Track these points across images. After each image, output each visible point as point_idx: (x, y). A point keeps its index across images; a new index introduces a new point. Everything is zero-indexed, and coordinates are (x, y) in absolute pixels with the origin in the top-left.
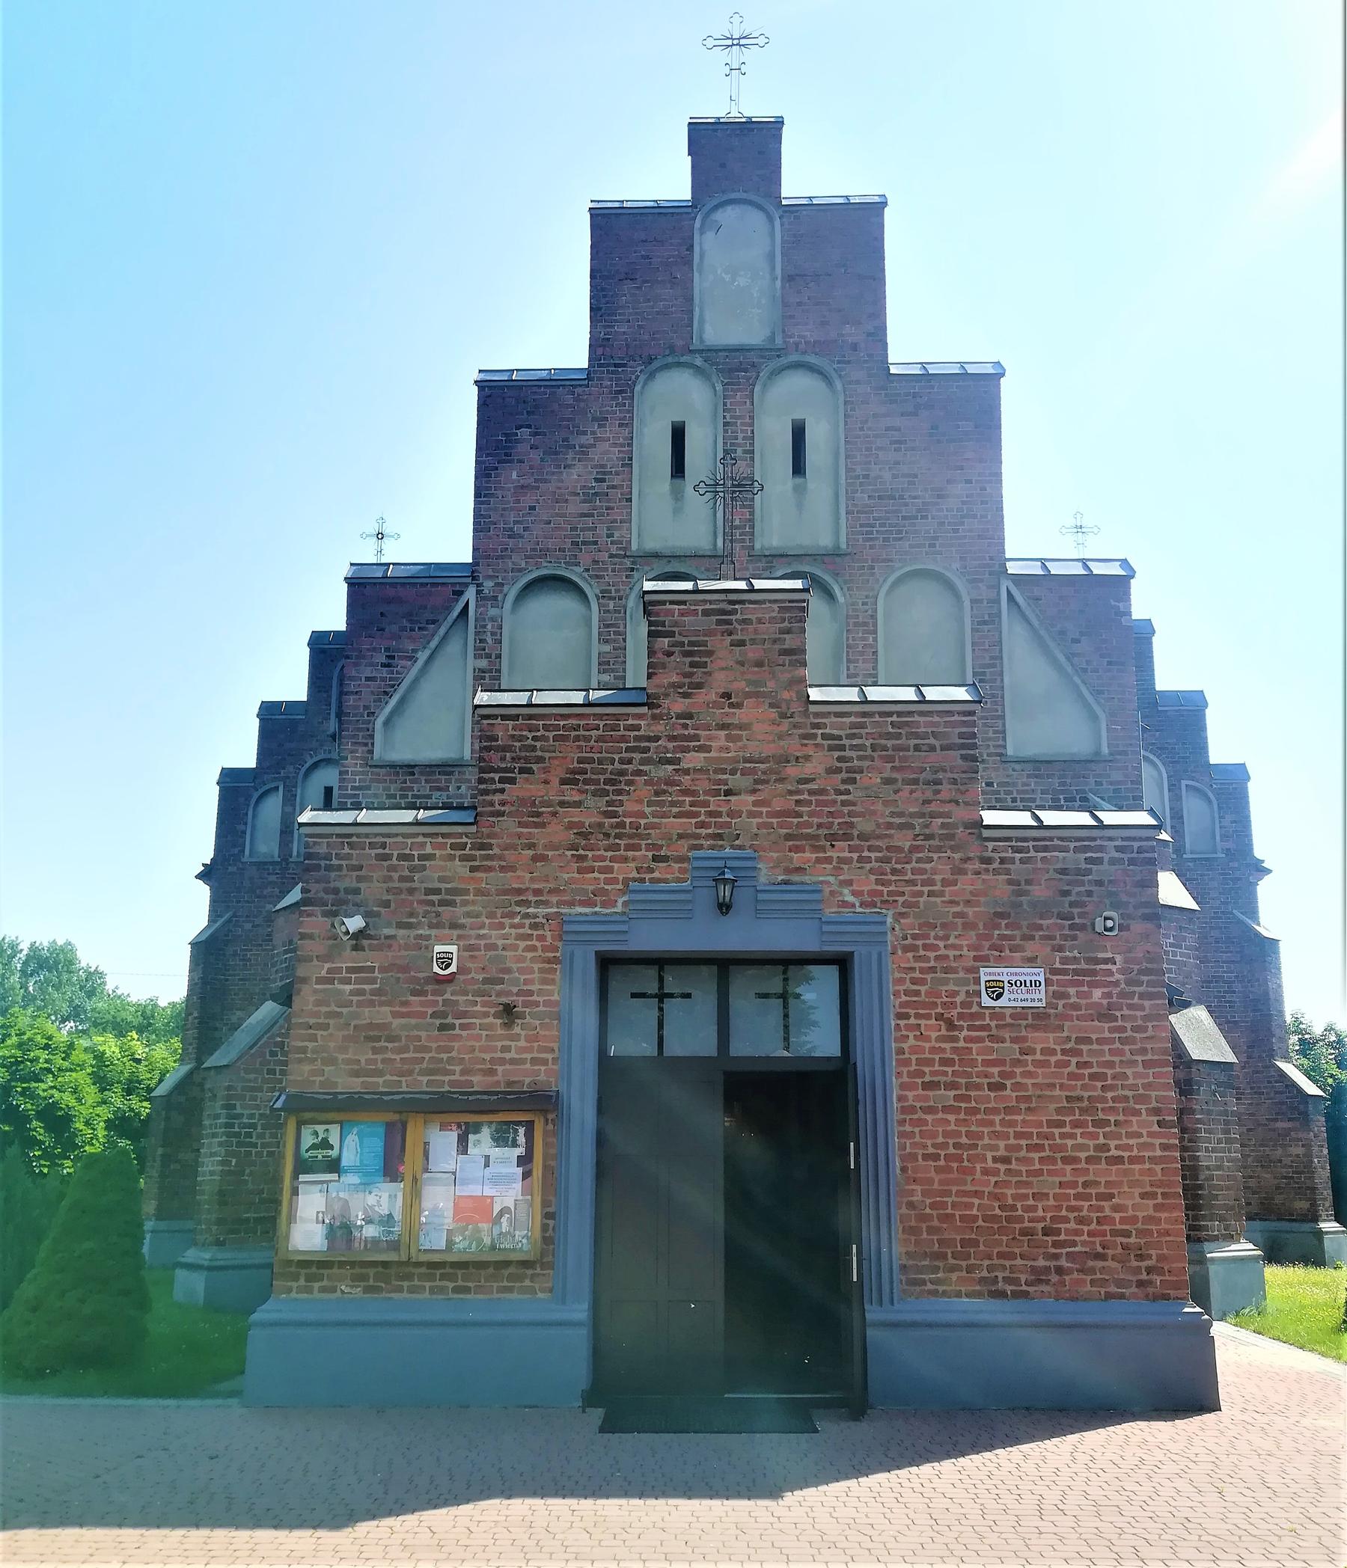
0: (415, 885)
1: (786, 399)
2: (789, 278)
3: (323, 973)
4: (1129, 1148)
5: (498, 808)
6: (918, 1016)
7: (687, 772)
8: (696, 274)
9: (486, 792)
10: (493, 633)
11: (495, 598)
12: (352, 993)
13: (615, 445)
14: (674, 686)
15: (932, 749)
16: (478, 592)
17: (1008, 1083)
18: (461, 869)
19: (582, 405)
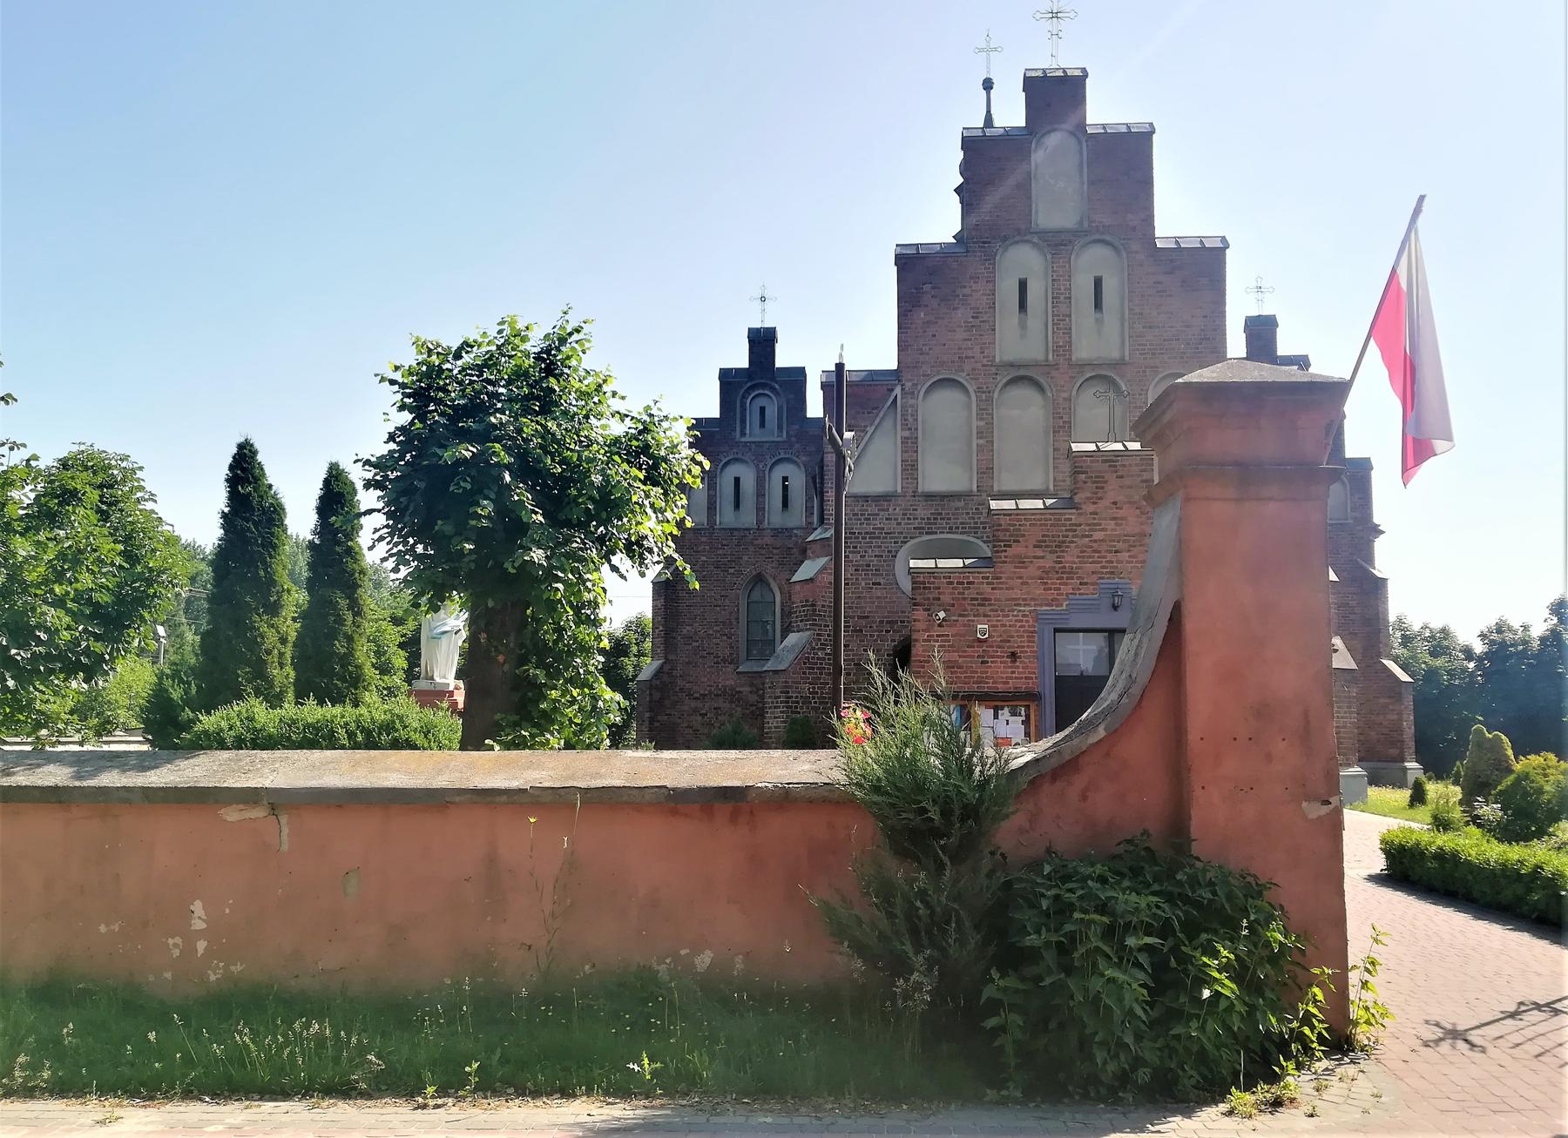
1: (1091, 262)
2: (1091, 183)
18: (988, 589)
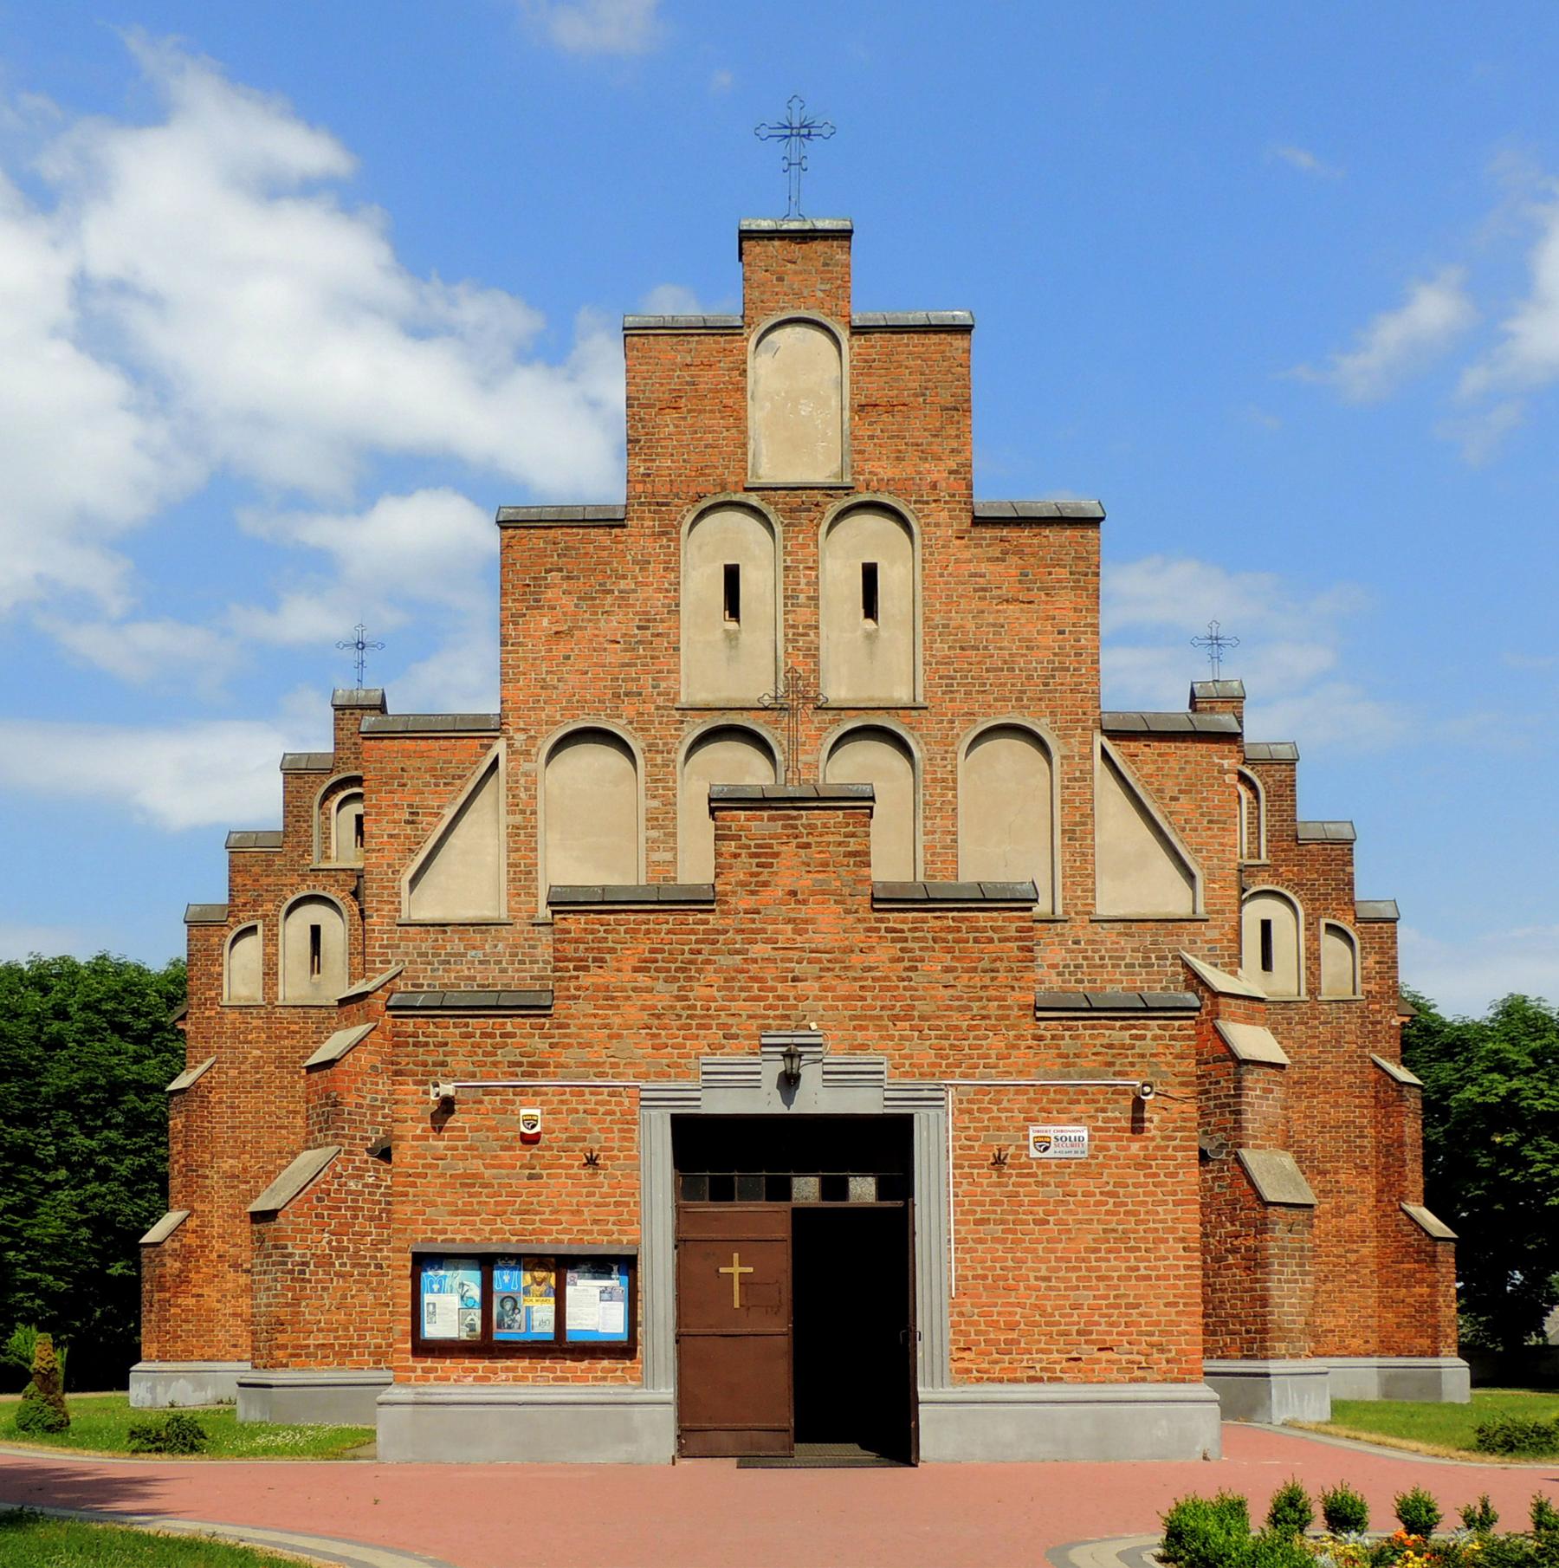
0: (499, 1058)
2: (861, 408)
3: (418, 1132)
4: (1156, 1268)
5: (573, 992)
6: (970, 1167)
7: (755, 961)
8: (749, 401)
9: (561, 979)
10: (527, 789)
11: (528, 753)
12: (447, 1148)
13: (659, 590)
14: (742, 884)
15: (991, 940)
16: (509, 746)
17: (1051, 1219)
19: (620, 546)
